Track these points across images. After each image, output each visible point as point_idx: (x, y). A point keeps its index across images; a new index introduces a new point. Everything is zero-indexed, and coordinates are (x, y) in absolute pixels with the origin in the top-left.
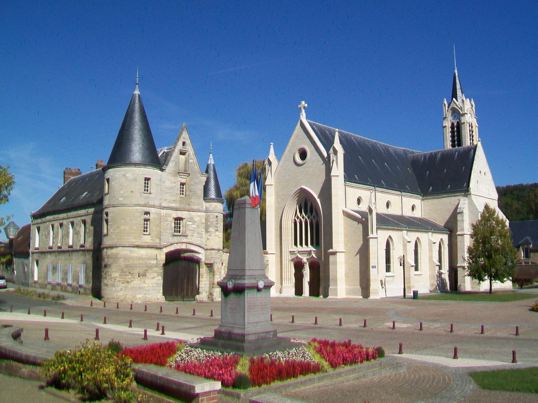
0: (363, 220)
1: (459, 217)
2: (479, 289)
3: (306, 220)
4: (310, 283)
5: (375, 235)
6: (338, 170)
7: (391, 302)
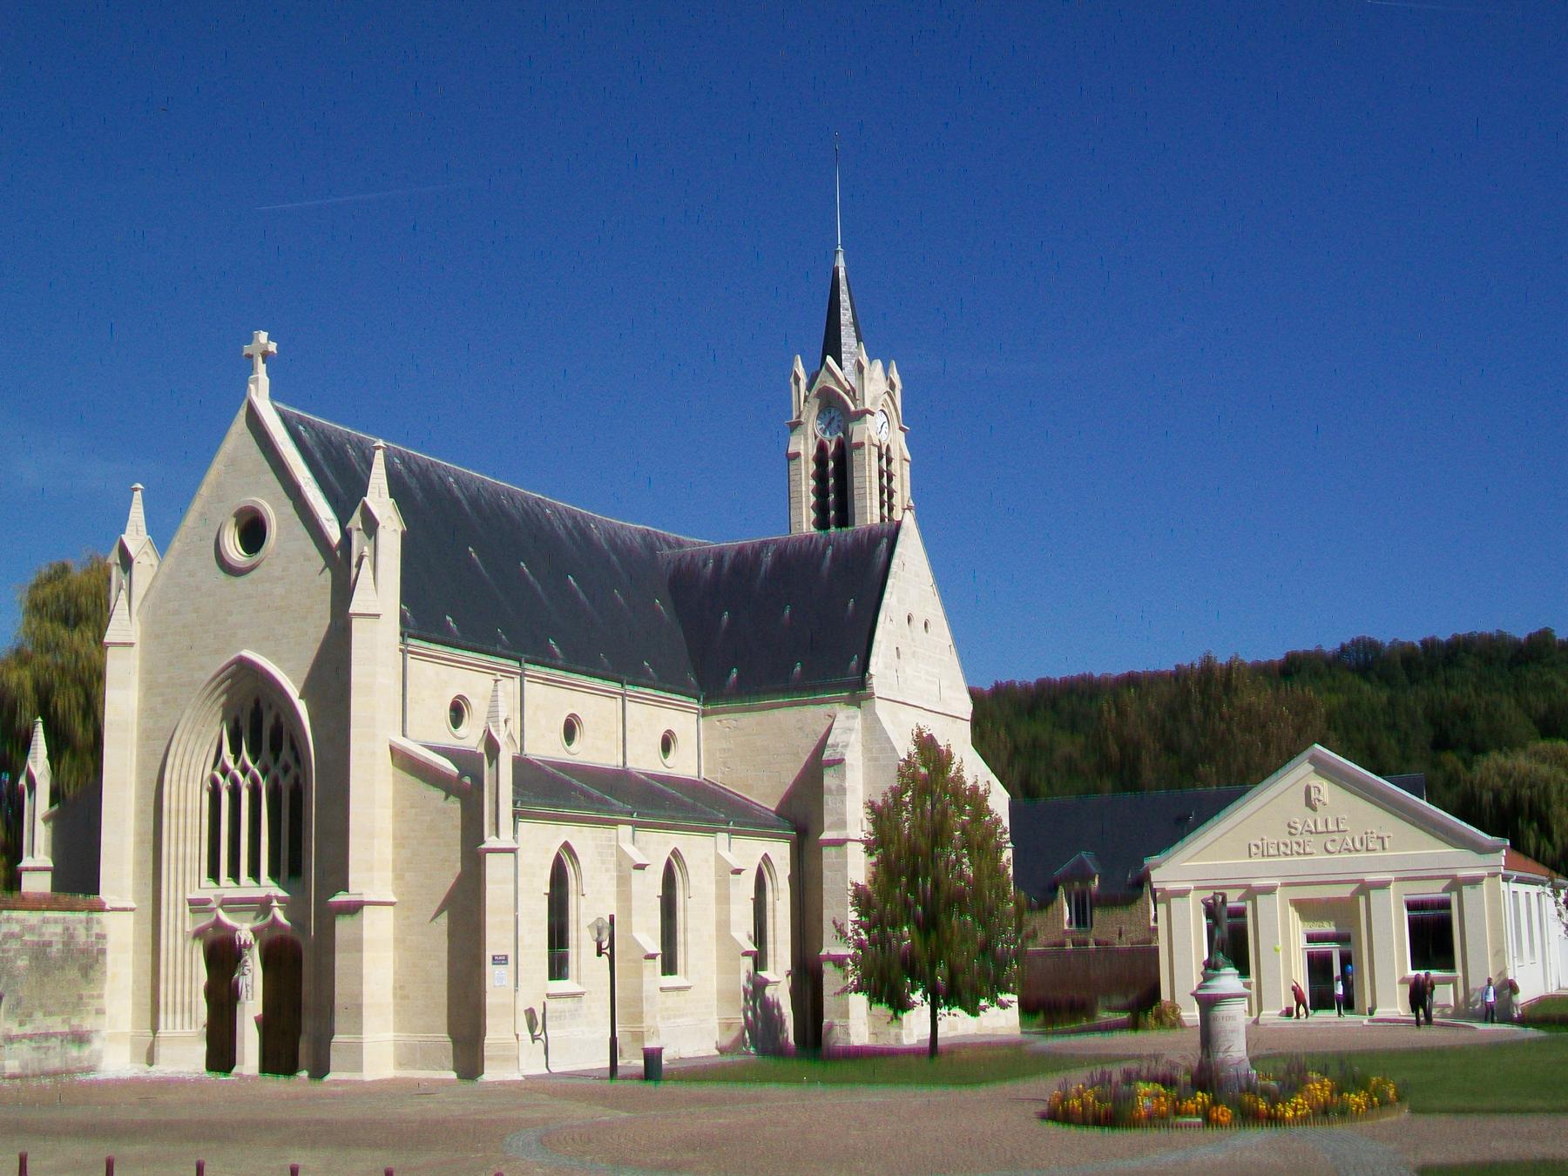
0: (461, 783)
1: (829, 780)
2: (898, 1037)
3: (255, 780)
4: (266, 1025)
5: (505, 840)
6: (379, 593)
7: (554, 1093)
